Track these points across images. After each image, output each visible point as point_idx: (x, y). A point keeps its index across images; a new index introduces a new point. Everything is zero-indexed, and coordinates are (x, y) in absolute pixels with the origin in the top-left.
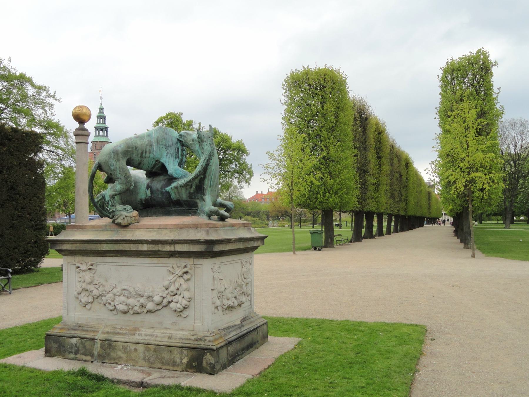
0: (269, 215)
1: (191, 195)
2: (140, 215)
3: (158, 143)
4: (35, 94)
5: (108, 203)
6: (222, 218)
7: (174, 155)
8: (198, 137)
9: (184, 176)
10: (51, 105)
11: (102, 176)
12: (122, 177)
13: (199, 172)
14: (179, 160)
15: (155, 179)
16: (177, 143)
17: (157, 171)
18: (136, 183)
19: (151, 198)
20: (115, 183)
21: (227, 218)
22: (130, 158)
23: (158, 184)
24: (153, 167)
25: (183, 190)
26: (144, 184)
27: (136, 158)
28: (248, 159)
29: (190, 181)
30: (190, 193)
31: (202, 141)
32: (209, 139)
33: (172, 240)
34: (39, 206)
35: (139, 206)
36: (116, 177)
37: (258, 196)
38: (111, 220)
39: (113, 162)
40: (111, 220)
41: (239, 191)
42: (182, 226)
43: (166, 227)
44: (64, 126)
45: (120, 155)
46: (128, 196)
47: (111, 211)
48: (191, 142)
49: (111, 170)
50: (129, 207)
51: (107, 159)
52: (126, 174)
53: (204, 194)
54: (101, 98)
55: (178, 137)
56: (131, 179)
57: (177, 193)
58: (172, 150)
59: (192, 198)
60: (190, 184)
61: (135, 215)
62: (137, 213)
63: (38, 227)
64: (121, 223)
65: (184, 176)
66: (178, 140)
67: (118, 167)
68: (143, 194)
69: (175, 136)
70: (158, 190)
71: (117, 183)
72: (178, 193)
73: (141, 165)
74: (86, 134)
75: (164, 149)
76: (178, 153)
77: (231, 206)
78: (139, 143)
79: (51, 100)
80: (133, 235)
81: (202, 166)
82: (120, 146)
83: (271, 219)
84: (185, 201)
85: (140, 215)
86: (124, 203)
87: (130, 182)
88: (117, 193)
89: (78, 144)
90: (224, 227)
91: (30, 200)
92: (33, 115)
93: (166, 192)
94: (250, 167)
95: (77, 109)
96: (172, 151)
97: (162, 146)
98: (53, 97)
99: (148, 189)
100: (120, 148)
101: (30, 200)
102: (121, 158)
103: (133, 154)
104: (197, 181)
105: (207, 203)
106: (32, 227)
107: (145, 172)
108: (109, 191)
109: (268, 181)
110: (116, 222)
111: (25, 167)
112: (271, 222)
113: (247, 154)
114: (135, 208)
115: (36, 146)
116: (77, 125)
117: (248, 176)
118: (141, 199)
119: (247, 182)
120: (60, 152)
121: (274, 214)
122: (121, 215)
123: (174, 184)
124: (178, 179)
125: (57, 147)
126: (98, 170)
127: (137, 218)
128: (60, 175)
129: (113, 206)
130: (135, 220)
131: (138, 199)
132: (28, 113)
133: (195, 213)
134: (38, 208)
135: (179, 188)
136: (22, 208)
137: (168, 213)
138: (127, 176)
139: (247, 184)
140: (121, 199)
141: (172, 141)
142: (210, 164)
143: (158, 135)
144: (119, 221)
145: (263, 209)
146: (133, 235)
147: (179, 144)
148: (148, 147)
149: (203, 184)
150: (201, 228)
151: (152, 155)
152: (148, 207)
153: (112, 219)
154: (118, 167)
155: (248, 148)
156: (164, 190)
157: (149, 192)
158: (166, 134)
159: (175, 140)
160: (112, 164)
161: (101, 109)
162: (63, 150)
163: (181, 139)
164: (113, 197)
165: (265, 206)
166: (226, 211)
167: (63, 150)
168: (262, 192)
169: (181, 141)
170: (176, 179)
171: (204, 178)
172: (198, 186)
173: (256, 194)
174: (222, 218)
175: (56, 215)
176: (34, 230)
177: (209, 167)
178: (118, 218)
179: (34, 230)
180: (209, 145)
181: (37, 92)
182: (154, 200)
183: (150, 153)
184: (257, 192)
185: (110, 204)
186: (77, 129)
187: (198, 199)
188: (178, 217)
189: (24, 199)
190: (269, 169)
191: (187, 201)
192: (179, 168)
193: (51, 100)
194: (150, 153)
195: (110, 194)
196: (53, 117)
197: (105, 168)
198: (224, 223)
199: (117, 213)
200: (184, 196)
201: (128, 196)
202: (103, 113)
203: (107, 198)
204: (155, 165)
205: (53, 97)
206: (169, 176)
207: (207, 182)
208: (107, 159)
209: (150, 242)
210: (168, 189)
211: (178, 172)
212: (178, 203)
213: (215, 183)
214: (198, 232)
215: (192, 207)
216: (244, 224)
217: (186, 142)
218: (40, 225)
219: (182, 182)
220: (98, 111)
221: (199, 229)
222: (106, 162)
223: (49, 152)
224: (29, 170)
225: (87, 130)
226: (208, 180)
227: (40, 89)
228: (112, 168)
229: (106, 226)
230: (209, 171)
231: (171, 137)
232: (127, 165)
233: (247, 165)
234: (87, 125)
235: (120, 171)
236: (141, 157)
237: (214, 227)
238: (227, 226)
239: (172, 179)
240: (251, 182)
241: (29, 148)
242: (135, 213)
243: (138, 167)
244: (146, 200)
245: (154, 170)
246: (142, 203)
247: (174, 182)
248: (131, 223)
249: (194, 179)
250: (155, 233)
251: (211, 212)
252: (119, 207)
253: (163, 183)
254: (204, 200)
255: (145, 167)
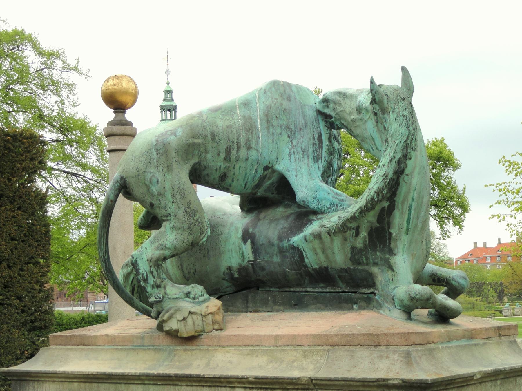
0: (502, 291)
1: (356, 255)
2: (227, 308)
3: (268, 122)
4: (43, 66)
5: (146, 280)
6: (443, 316)
7: (311, 150)
8: (373, 101)
9: (335, 203)
10: (70, 86)
11: (129, 212)
12: (180, 213)
13: (378, 193)
14: (322, 164)
15: (262, 215)
16: (317, 121)
17: (269, 195)
18: (216, 227)
19: (253, 263)
20: (162, 229)
21: (455, 314)
22: (199, 163)
23: (271, 227)
24: (258, 186)
25: (337, 242)
26: (237, 229)
27: (214, 162)
28: (459, 178)
29: (353, 218)
30: (353, 248)
31: (384, 111)
32: (401, 104)
33: (311, 379)
34: (37, 282)
35: (226, 284)
36: (165, 213)
37: (479, 253)
38: (154, 323)
39: (156, 174)
40: (154, 323)
41: (439, 244)
42: (336, 340)
43: (292, 343)
44: (96, 125)
45: (174, 156)
46: (196, 260)
47: (152, 299)
48: (355, 116)
49: (152, 195)
50: (198, 289)
51: (141, 165)
52: (189, 203)
53: (391, 252)
54: (168, 72)
55: (319, 107)
56: (203, 217)
57: (319, 251)
58: (305, 140)
59: (359, 263)
60: (354, 225)
61: (213, 309)
62: (219, 303)
63: (37, 324)
64: (177, 331)
65: (336, 206)
66: (319, 112)
67: (168, 185)
68: (235, 254)
69: (312, 103)
70: (271, 245)
71: (166, 226)
72: (324, 251)
73: (229, 181)
74: (128, 132)
75: (285, 137)
76: (321, 147)
77: (462, 282)
78: (221, 124)
79: (71, 77)
80: (208, 364)
81: (386, 175)
82: (174, 133)
83: (506, 299)
84: (342, 270)
85: (227, 308)
86: (187, 280)
87: (198, 223)
88: (167, 253)
89: (113, 154)
90: (450, 340)
91: (21, 270)
92: (39, 109)
93: (293, 247)
94: (461, 192)
95: (111, 82)
96: (305, 140)
97: (279, 131)
98: (76, 69)
99: (245, 242)
100: (173, 137)
101: (21, 270)
102: (175, 165)
103: (206, 151)
104: (372, 217)
105: (400, 278)
106: (24, 324)
107: (236, 199)
108: (148, 248)
109: (509, 220)
110: (166, 328)
111: (12, 203)
112: (507, 305)
113: (456, 167)
114: (214, 292)
115: (32, 159)
116: (110, 114)
117: (457, 212)
118: (229, 268)
119: (458, 223)
120: (89, 175)
121: (513, 289)
122: (178, 310)
123: (313, 228)
124: (322, 213)
125: (84, 167)
126: (121, 195)
127: (219, 318)
128: (89, 220)
129: (158, 286)
130: (214, 322)
131: (223, 268)
132: (30, 105)
133: (368, 302)
134: (37, 287)
135: (326, 238)
136: (6, 287)
137: (298, 304)
138: (193, 210)
139: (457, 227)
140: (181, 268)
141: (304, 116)
142: (407, 171)
143: (268, 103)
144: (173, 325)
145: (490, 279)
146: (208, 364)
147: (322, 124)
148: (243, 134)
149: (389, 225)
150: (388, 345)
151: (253, 155)
152: (245, 287)
153: (156, 318)
154: (168, 185)
155: (458, 156)
156: (285, 244)
157: (247, 249)
158: (289, 98)
159: (311, 114)
160: (154, 180)
161: (168, 92)
162: (95, 171)
163: (327, 111)
164: (157, 263)
165: (493, 271)
166: (447, 293)
167: (95, 171)
168: (485, 244)
169: (326, 117)
170: (315, 212)
171: (391, 209)
172: (378, 227)
173: (472, 247)
174: (443, 316)
175: (90, 296)
176: (30, 331)
177: (404, 179)
178: (170, 317)
179: (30, 331)
180: (401, 119)
181: (45, 63)
182: (263, 269)
183: (249, 148)
184: (475, 244)
185: (151, 281)
186: (111, 124)
187: (375, 264)
188: (324, 313)
189: (9, 267)
190: (509, 194)
191: (346, 271)
192: (324, 185)
193: (71, 77)
194: (249, 148)
195: (150, 255)
196: (76, 109)
197: (137, 191)
198: (450, 328)
199: (167, 305)
200: (339, 257)
201: (196, 260)
202: (171, 99)
203: (144, 267)
204: (263, 179)
205: (76, 69)
206: (299, 206)
207: (398, 219)
208: (141, 165)
209: (251, 383)
210: (296, 240)
211: (321, 195)
212: (323, 276)
213: (421, 220)
214: (381, 357)
215: (358, 286)
216: (499, 328)
217: (340, 118)
218: (40, 320)
219: (333, 220)
220: (162, 96)
221: (382, 348)
222: (140, 175)
223: (70, 176)
224: (19, 208)
225: (130, 124)
226: (402, 213)
227: (51, 55)
228: (154, 189)
229: (142, 337)
230: (403, 189)
231: (302, 107)
232: (193, 182)
233: (454, 189)
234: (129, 115)
235: (173, 196)
236: (227, 158)
237: (424, 341)
238: (458, 338)
239: (306, 214)
240: (464, 224)
241: (18, 165)
242: (214, 304)
243: (221, 183)
244: (242, 269)
245: (260, 193)
246: (232, 278)
247: (310, 222)
248: (204, 331)
249: (364, 211)
250: (265, 358)
251: (412, 299)
252: (173, 290)
253: (283, 224)
254: (391, 268)
255: (238, 184)
